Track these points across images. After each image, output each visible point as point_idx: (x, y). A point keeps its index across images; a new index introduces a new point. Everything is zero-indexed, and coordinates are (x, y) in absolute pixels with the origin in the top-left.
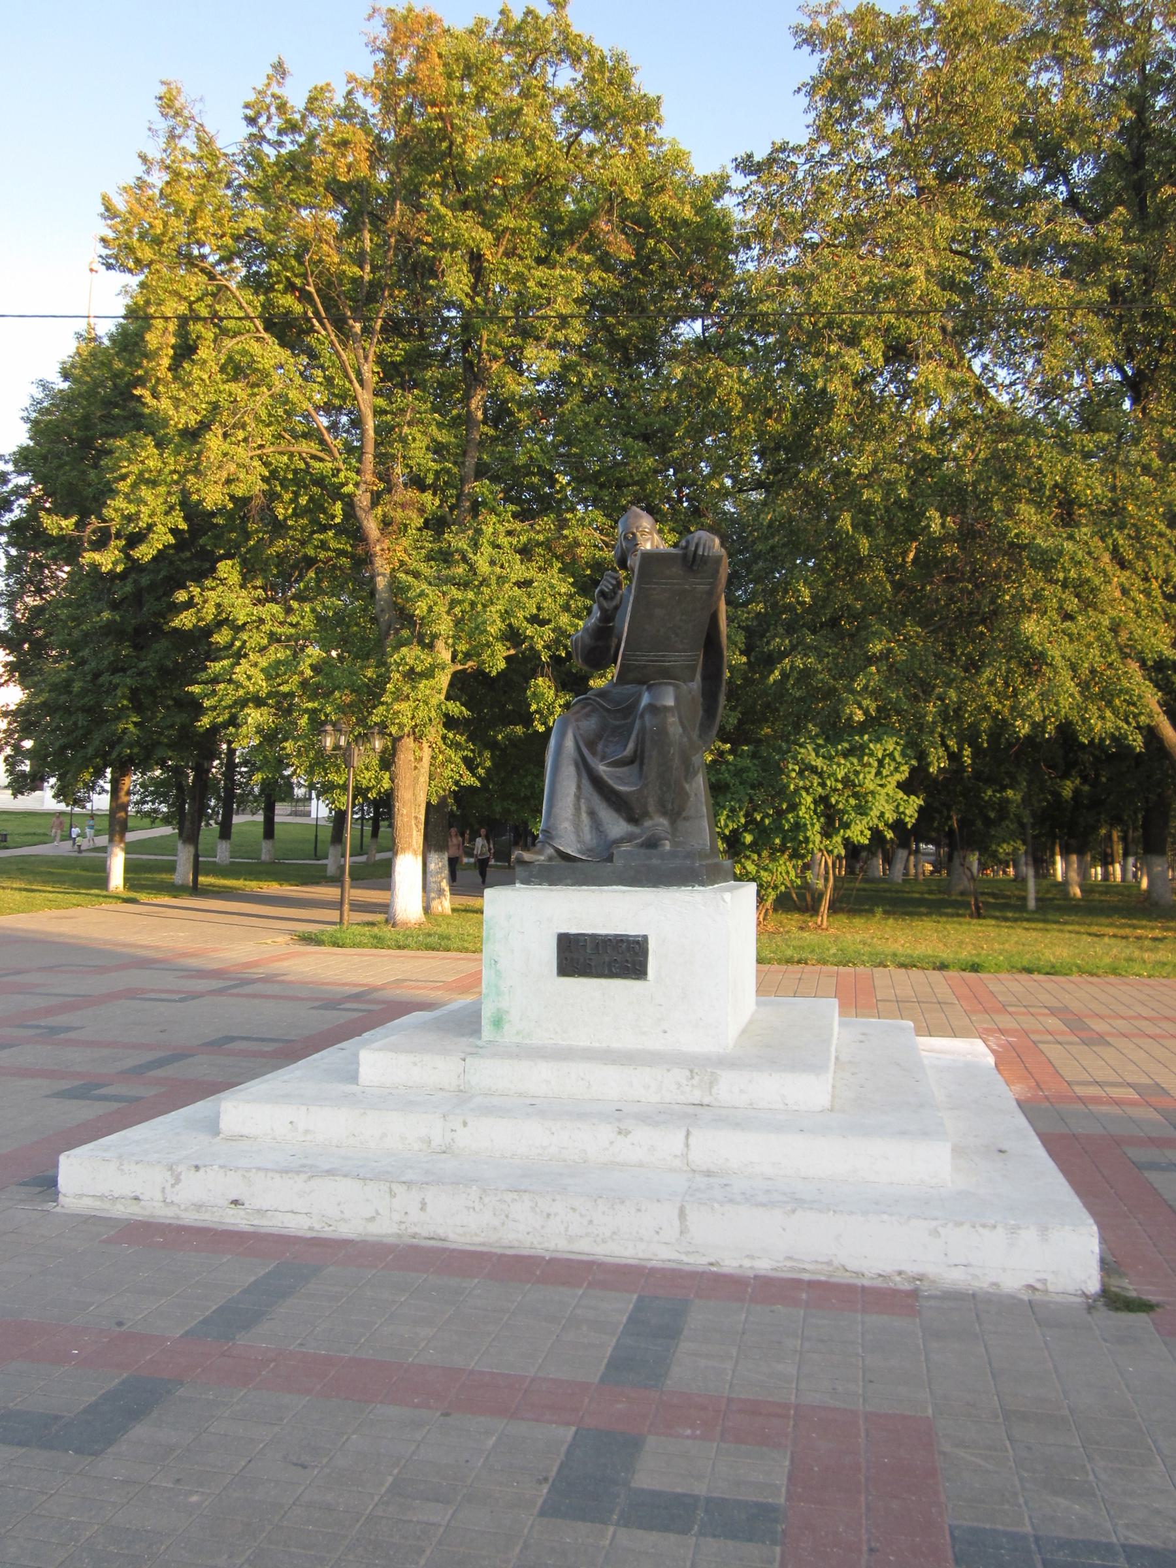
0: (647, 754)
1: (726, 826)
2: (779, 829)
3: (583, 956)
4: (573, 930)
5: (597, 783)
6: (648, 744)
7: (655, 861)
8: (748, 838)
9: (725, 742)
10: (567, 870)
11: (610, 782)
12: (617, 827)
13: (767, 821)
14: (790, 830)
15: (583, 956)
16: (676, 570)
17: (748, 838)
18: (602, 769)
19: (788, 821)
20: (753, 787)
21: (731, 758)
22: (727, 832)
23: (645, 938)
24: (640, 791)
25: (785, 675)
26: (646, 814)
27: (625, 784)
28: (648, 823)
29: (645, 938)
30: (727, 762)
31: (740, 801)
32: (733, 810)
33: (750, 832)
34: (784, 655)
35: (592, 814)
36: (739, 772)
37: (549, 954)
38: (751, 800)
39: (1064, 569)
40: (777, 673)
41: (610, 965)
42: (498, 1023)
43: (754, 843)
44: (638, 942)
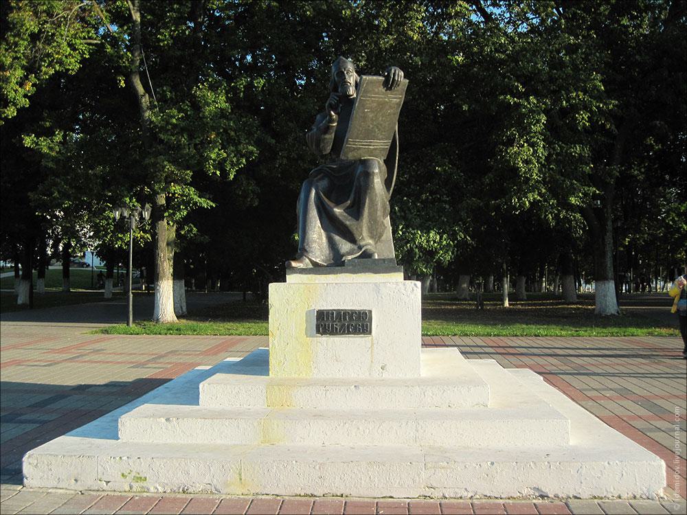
3: (332, 323)
15: (332, 323)
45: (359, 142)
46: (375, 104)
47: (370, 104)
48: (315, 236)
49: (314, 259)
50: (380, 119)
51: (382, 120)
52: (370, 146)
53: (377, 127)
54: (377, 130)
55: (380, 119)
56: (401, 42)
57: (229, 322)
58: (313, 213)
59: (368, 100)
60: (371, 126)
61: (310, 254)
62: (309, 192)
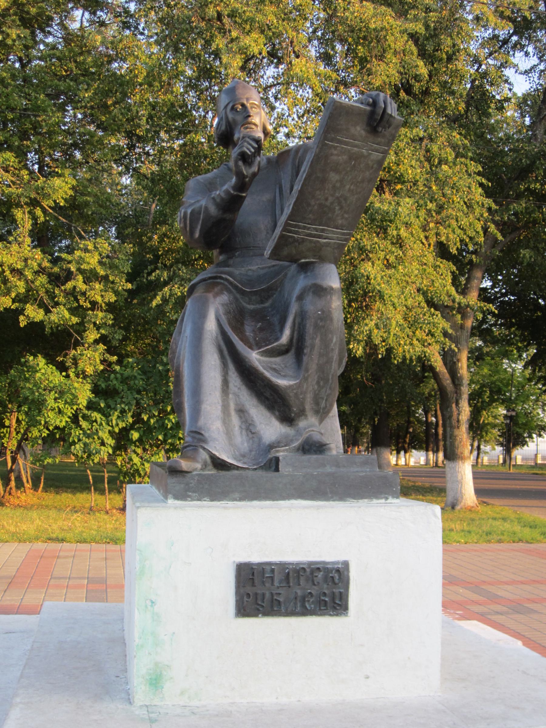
0: (308, 342)
1: (117, 425)
2: (163, 427)
3: (274, 591)
4: (255, 558)
5: (251, 378)
6: (310, 328)
7: (329, 469)
8: (135, 435)
9: (112, 354)
10: (221, 480)
11: (267, 374)
12: (270, 428)
13: (152, 421)
14: (171, 428)
15: (274, 591)
16: (359, 130)
17: (135, 435)
18: (255, 357)
19: (170, 420)
20: (139, 392)
21: (118, 368)
22: (117, 430)
23: (346, 564)
24: (299, 385)
25: (165, 301)
26: (302, 413)
27: (284, 377)
28: (302, 424)
29: (346, 564)
30: (114, 372)
31: (128, 404)
32: (123, 412)
33: (138, 430)
34: (166, 283)
35: (241, 411)
36: (125, 380)
37: (224, 590)
38: (138, 404)
39: (397, 228)
40: (158, 298)
41: (303, 599)
42: (156, 681)
43: (140, 440)
44: (338, 571)
45: (305, 228)
46: (345, 157)
47: (337, 155)
48: (517, 368)
49: (214, 452)
50: (348, 187)
51: (349, 190)
52: (320, 237)
53: (340, 203)
54: (337, 208)
55: (348, 187)
56: (123, 29)
57: (377, 498)
58: (212, 361)
59: (335, 148)
60: (330, 199)
61: (211, 443)
62: (202, 316)
